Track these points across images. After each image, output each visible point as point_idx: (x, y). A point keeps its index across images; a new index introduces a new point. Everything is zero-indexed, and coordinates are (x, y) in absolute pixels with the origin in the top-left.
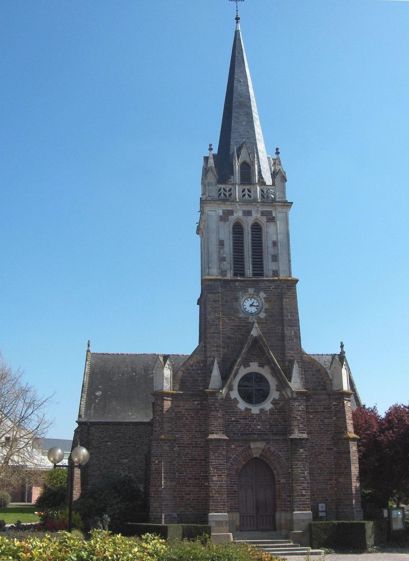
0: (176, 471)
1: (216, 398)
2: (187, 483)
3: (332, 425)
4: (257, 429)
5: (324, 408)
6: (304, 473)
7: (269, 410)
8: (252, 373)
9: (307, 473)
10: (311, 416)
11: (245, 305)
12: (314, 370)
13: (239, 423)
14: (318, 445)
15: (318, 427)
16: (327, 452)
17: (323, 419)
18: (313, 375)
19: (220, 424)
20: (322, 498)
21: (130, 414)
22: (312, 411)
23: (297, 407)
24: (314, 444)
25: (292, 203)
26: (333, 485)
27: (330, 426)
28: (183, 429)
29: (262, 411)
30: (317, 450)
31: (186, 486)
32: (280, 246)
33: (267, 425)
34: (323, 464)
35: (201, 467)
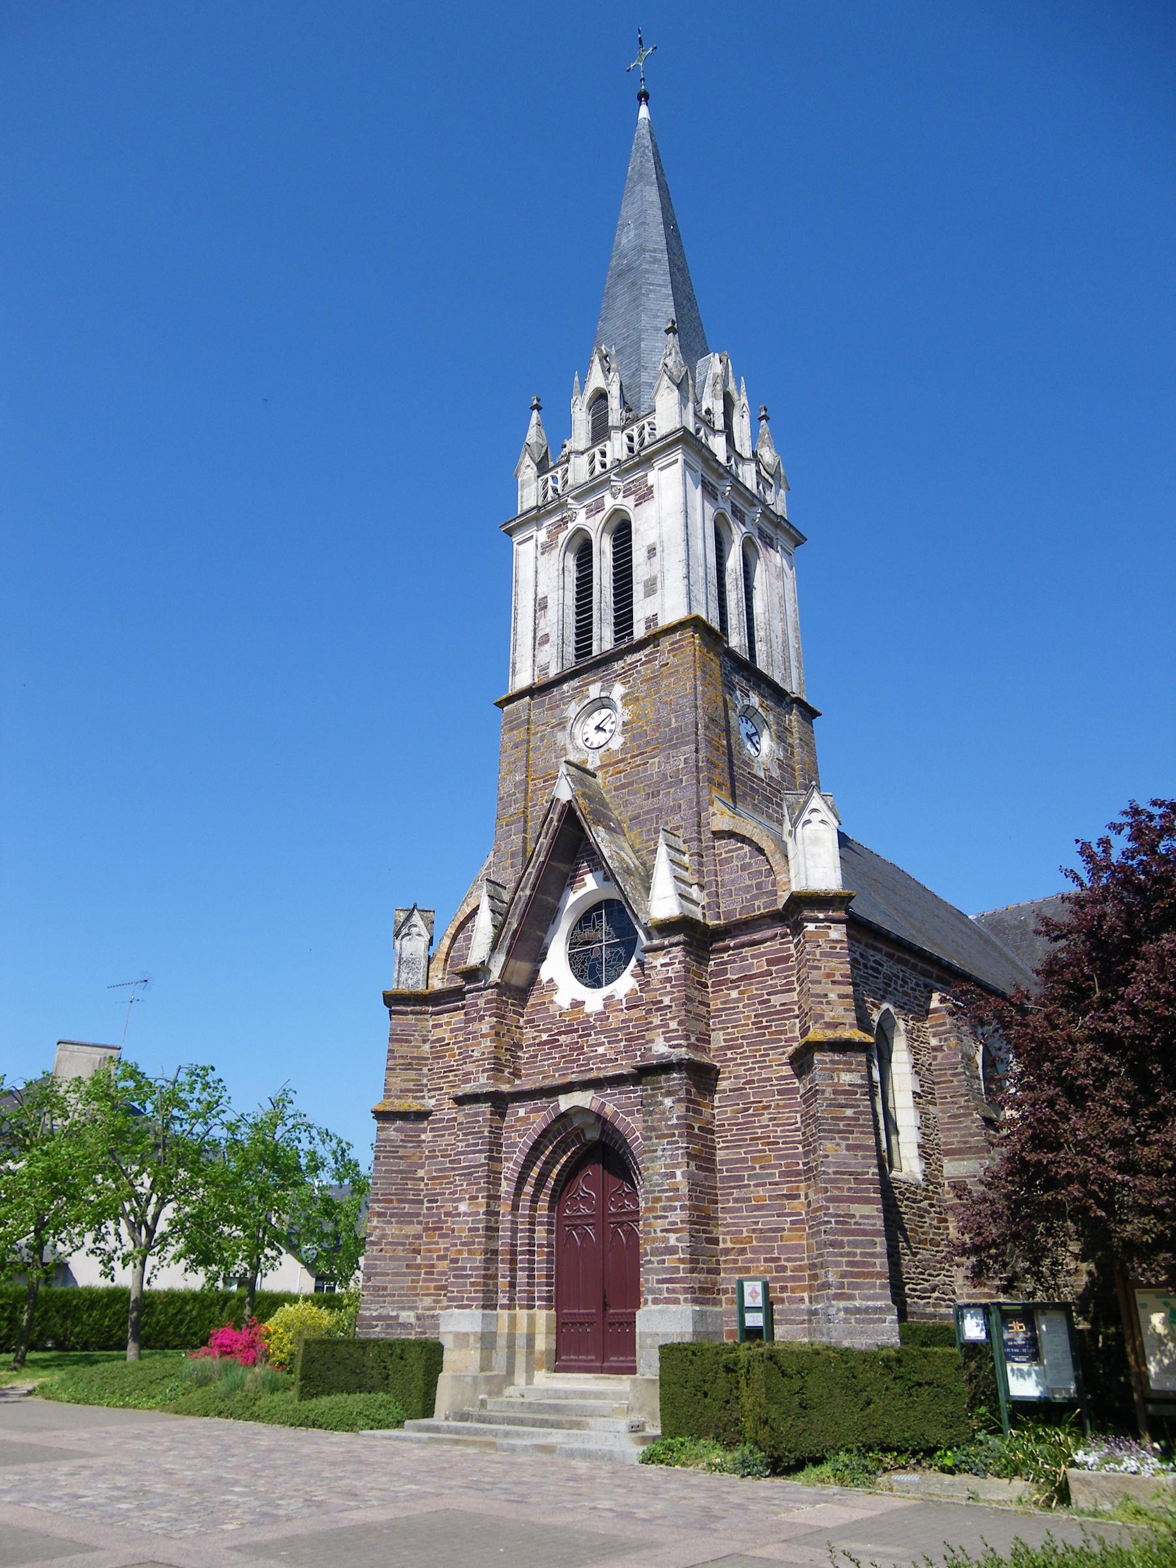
0: (425, 1196)
1: (713, 1236)
2: (868, 1173)
3: (793, 1010)
4: (596, 1057)
5: (770, 962)
6: (673, 1175)
7: (625, 996)
8: (601, 902)
9: (682, 1173)
10: (734, 994)
11: (592, 743)
12: (745, 853)
13: (556, 1047)
14: (753, 1082)
15: (753, 1023)
16: (781, 1103)
17: (766, 997)
18: (744, 867)
19: (483, 1053)
20: (766, 1260)
21: (1142, 877)
22: (734, 977)
23: (664, 969)
24: (743, 1081)
25: (819, 714)
26: (801, 1214)
27: (528, 1189)
28: (444, 1083)
29: (609, 1000)
30: (752, 1099)
31: (442, 1236)
32: (548, 1449)
33: (621, 1040)
34: (769, 1144)
35: (403, 1035)
